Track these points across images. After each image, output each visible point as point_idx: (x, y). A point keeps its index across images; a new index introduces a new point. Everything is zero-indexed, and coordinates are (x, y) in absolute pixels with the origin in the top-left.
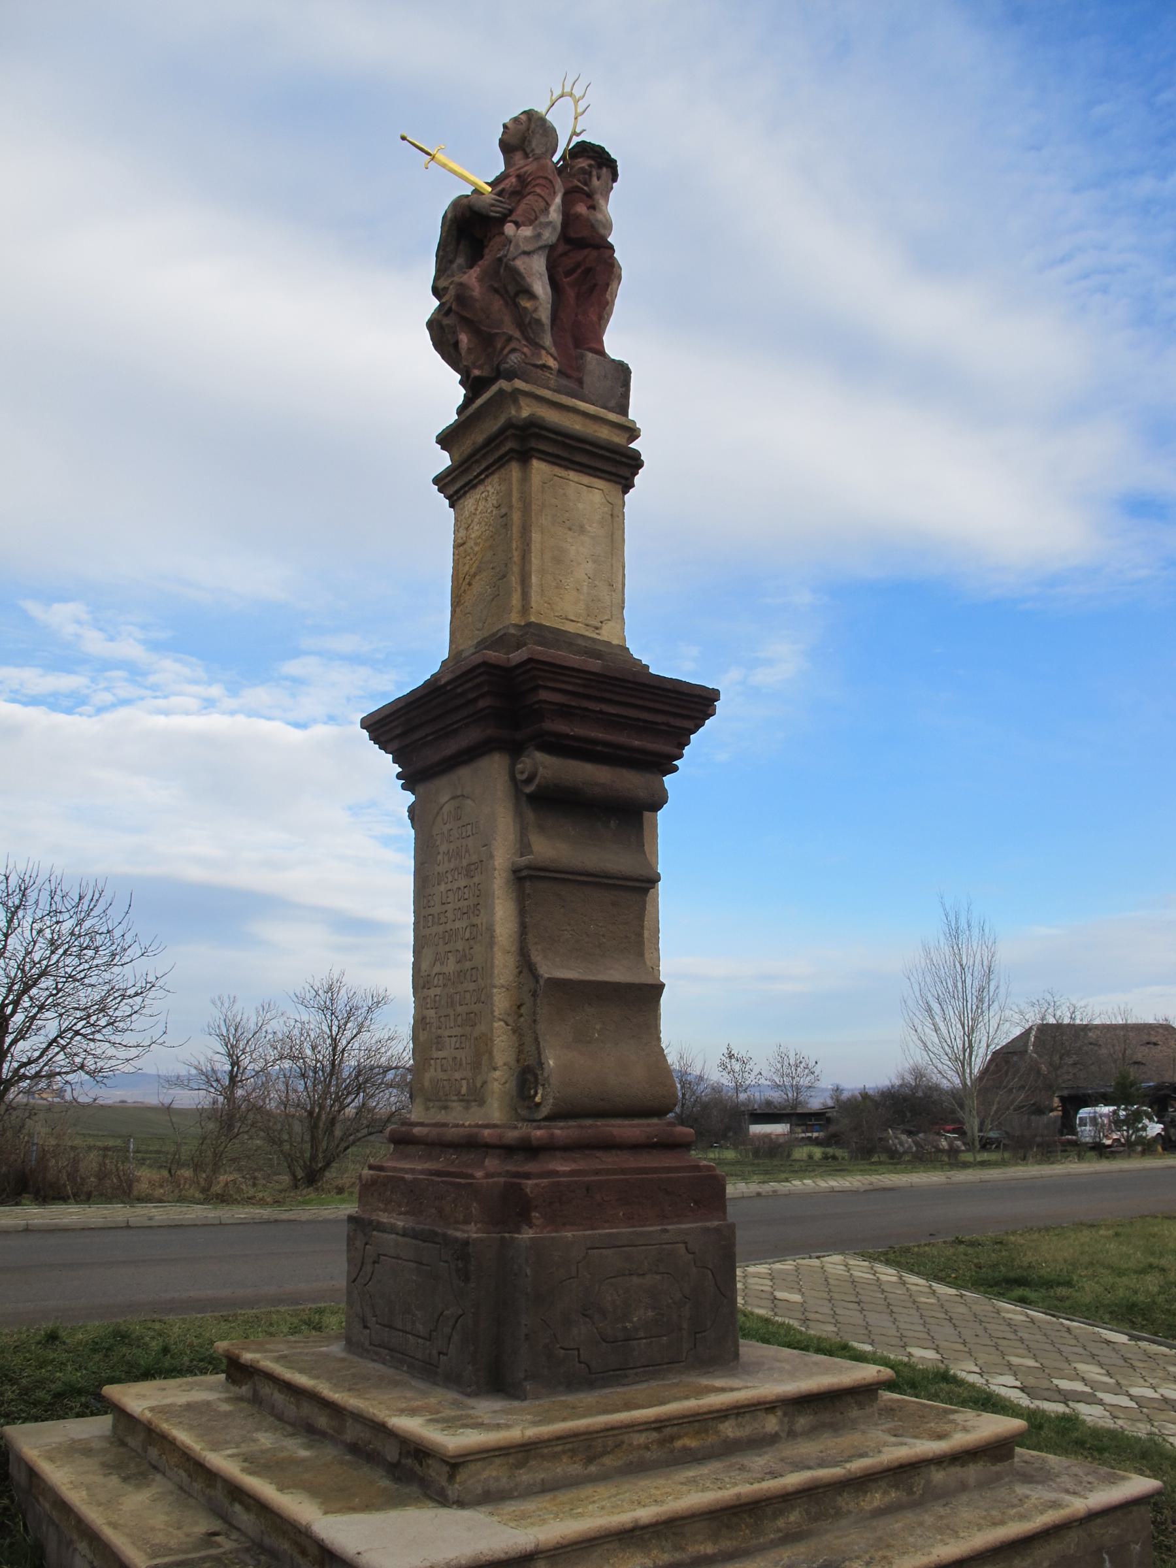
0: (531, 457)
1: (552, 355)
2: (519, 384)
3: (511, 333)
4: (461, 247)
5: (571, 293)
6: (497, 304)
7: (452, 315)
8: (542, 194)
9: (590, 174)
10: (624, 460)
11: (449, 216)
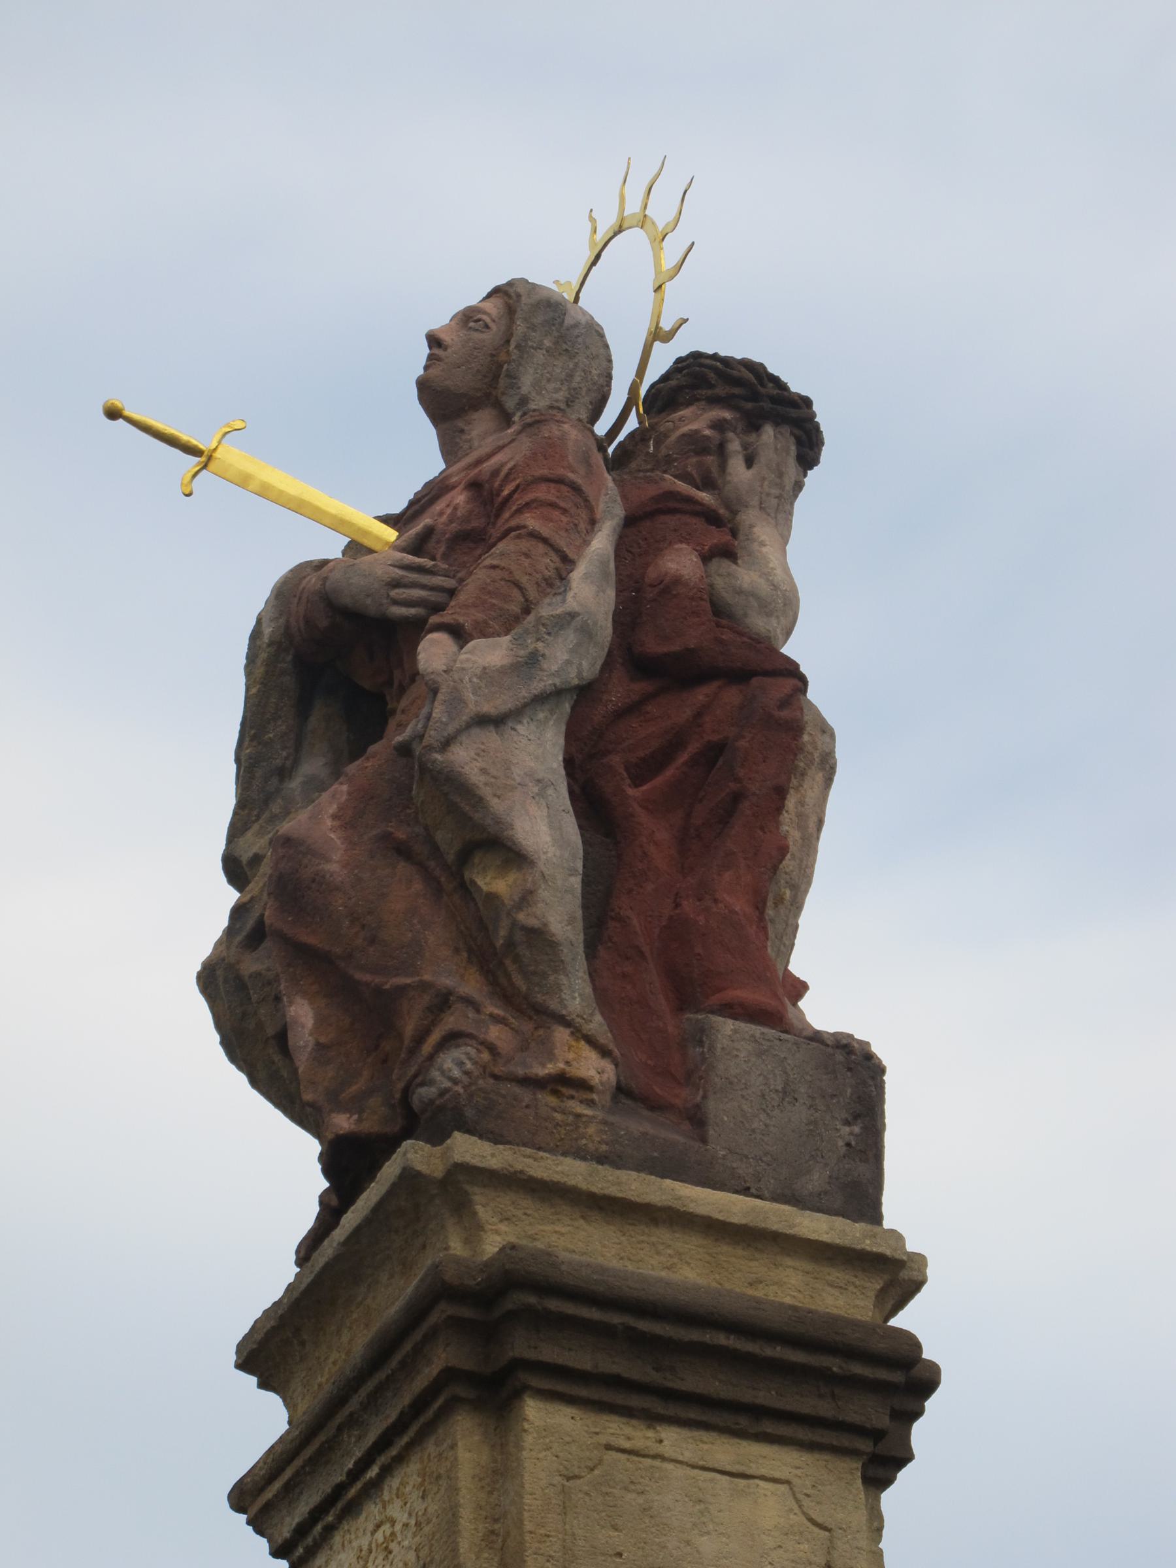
0: (518, 1394)
1: (591, 1041)
2: (467, 1148)
3: (446, 982)
4: (314, 721)
5: (655, 835)
6: (402, 893)
7: (267, 943)
8: (545, 531)
9: (721, 450)
10: (858, 1369)
11: (267, 631)
